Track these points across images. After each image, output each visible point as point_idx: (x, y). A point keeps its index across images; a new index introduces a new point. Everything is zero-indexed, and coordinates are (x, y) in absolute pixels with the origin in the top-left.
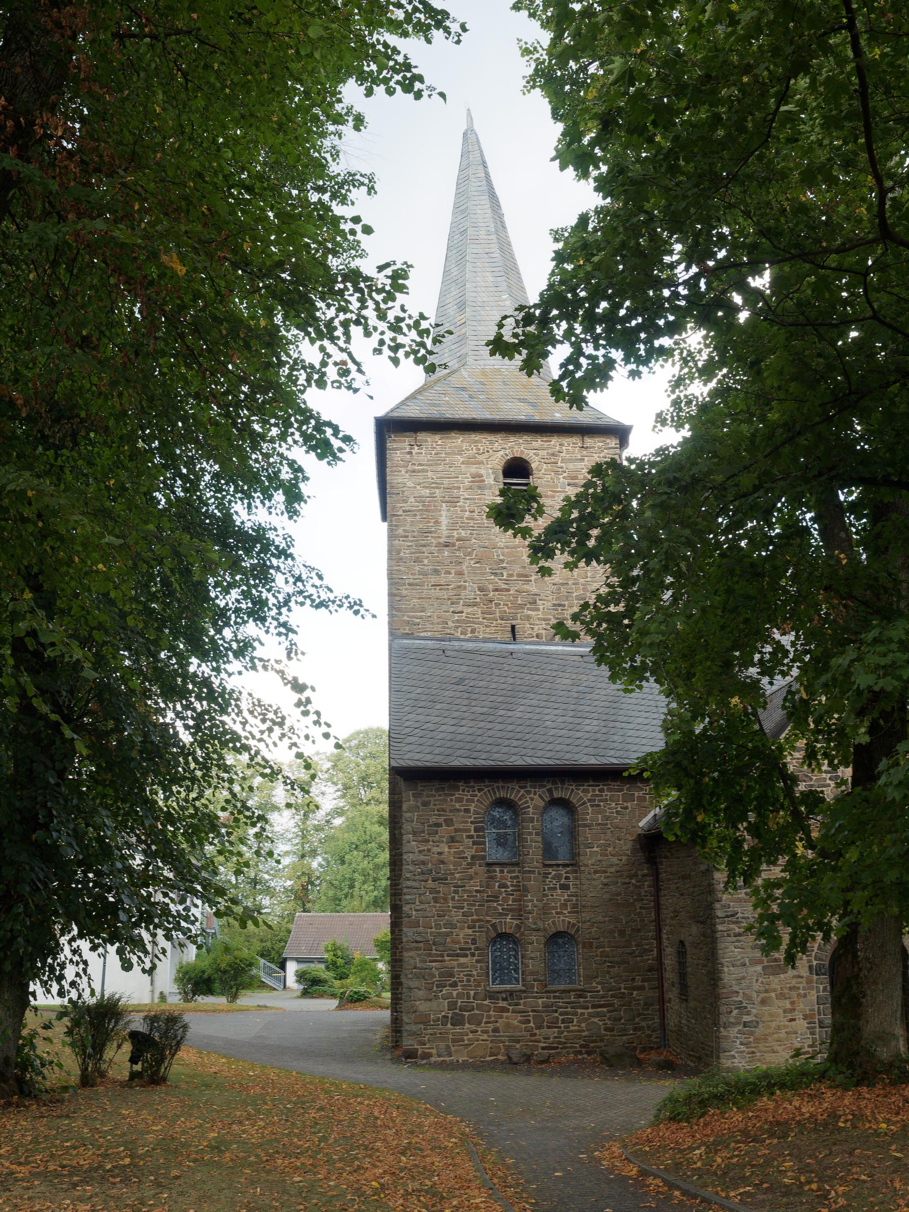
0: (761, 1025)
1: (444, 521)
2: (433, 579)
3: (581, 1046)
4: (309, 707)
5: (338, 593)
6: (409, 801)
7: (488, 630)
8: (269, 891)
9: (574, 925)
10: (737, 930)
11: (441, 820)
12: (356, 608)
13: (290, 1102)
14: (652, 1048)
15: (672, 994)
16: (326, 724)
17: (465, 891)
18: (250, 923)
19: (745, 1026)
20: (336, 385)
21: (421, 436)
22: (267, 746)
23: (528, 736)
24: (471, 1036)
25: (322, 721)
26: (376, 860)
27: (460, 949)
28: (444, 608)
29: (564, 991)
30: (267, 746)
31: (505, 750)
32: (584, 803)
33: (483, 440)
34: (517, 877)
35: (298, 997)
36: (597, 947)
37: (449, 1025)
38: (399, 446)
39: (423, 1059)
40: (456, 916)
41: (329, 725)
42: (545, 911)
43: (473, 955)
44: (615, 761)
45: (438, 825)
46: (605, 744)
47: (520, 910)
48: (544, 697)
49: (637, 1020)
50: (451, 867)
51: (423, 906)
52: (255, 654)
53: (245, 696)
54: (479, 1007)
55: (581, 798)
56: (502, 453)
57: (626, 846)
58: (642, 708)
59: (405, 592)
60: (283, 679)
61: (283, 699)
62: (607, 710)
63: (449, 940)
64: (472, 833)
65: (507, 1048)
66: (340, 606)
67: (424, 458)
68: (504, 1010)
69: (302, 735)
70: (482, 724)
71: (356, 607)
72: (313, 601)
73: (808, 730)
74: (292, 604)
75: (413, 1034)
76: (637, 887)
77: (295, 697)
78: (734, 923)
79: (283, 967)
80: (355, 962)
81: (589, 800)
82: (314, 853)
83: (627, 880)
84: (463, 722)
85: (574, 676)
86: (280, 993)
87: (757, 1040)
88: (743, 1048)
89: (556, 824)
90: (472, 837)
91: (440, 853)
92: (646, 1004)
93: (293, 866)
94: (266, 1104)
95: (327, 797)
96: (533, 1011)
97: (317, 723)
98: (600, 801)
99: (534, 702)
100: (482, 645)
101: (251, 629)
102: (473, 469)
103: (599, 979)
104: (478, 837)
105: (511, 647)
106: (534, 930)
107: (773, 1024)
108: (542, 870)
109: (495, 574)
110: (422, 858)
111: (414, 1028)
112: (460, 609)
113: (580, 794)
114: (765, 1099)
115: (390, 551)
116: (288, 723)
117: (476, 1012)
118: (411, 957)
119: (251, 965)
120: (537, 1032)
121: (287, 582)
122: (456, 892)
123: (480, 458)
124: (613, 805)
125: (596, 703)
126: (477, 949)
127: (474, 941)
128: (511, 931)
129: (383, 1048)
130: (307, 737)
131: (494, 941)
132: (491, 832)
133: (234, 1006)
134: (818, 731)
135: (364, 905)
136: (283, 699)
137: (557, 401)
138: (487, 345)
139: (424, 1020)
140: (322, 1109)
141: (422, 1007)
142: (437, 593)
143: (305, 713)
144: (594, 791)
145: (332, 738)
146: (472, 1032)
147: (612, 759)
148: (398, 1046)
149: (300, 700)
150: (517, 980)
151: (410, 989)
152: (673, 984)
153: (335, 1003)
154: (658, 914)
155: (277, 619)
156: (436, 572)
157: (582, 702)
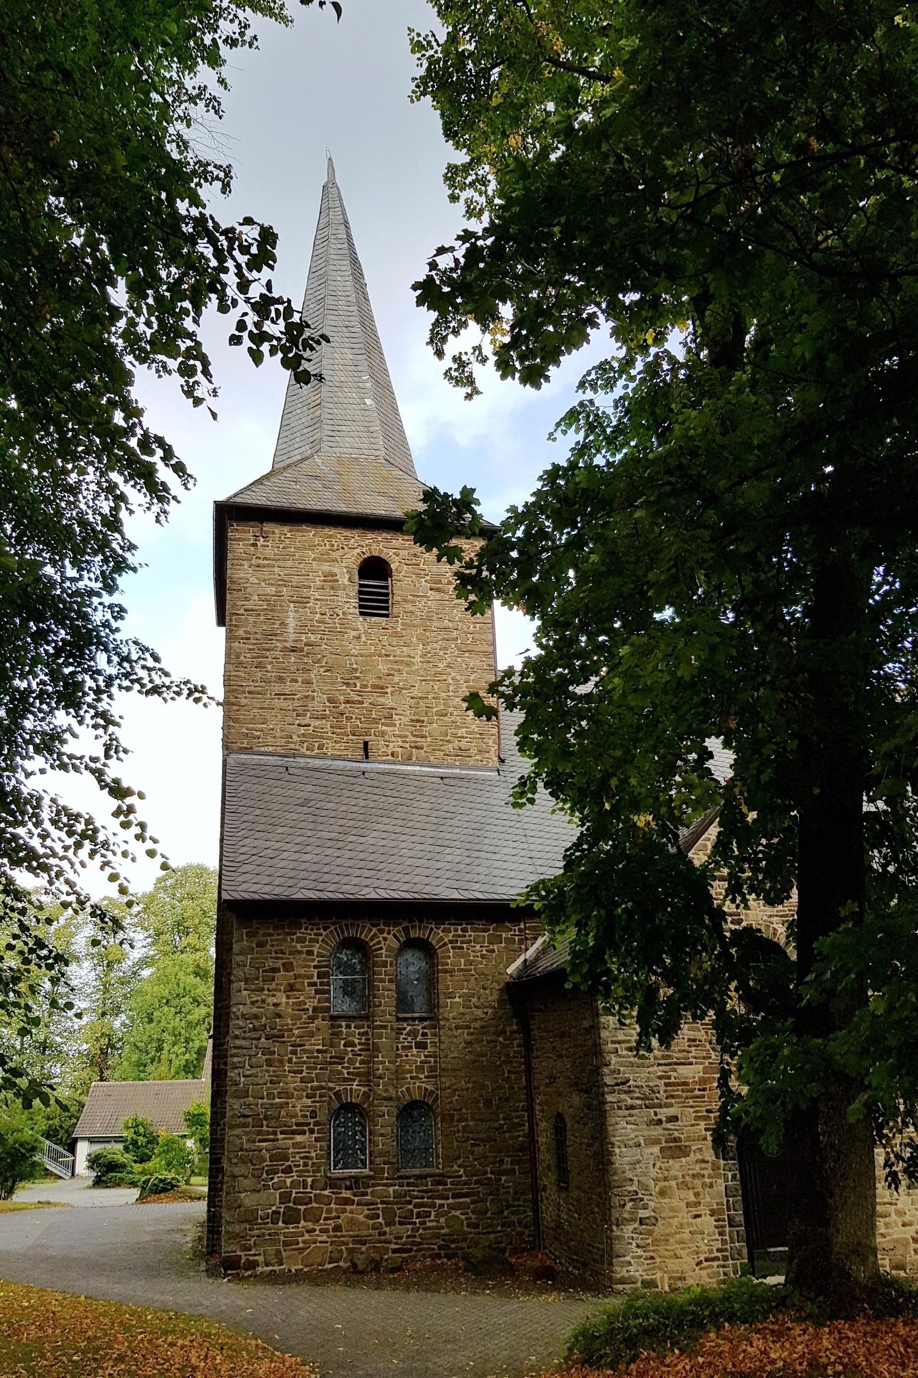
0: (660, 1222)
1: (292, 623)
2: (277, 688)
3: (440, 1248)
4: (131, 817)
5: (176, 677)
6: (241, 942)
7: (337, 746)
8: (60, 1056)
9: (432, 1092)
10: (629, 1102)
11: (279, 964)
12: (197, 695)
13: (77, 1350)
14: (524, 1250)
15: (548, 1180)
16: (151, 838)
17: (305, 1051)
18: (37, 1102)
19: (641, 1224)
20: (162, 518)
21: (268, 527)
22: (72, 864)
23: (381, 866)
24: (307, 1236)
25: (147, 835)
26: (189, 1017)
27: (297, 1124)
28: (289, 720)
29: (419, 1177)
30: (72, 864)
31: (356, 881)
32: (445, 945)
33: (338, 535)
34: (366, 1033)
35: (89, 1187)
36: (459, 1121)
37: (280, 1224)
38: (242, 538)
39: (247, 1270)
40: (293, 1082)
41: (155, 841)
42: (398, 1075)
43: (312, 1131)
44: (480, 896)
45: (275, 970)
46: (469, 877)
47: (369, 1074)
48: (400, 823)
49: (506, 1213)
50: (290, 1022)
51: (254, 1071)
52: (66, 749)
53: (46, 802)
54: (318, 1198)
55: (442, 939)
56: (358, 550)
57: (492, 996)
58: (509, 837)
59: (243, 701)
60: (100, 781)
61: (97, 805)
62: (470, 839)
63: (283, 1113)
64: (315, 979)
65: (351, 1251)
66: (178, 694)
67: (269, 552)
68: (347, 1202)
69: (119, 851)
70: (328, 852)
71: (196, 692)
72: (143, 686)
73: (732, 857)
74: (114, 690)
75: (234, 1236)
76: (506, 1046)
77: (114, 803)
78: (625, 1092)
79: (72, 1149)
80: (160, 1140)
81: (451, 942)
82: (117, 1011)
83: (493, 1038)
84: (308, 849)
85: (433, 800)
86: (67, 1183)
87: (656, 1242)
88: (640, 1252)
89: (411, 969)
90: (314, 984)
91: (276, 1005)
92: (516, 1192)
93: (91, 1026)
94: (43, 1357)
95: (139, 944)
96: (382, 1202)
97: (140, 837)
98: (463, 942)
99: (387, 828)
100: (330, 762)
101: (62, 718)
102: (326, 567)
103: (459, 1162)
104: (322, 984)
105: (363, 766)
106: (385, 1099)
107: (675, 1222)
108: (395, 1025)
109: (348, 684)
110: (255, 1010)
111: (237, 1228)
112: (306, 722)
113: (442, 935)
114: (712, 1335)
115: (228, 654)
116: (101, 837)
117: (315, 1205)
118: (236, 1137)
119: (34, 1149)
120: (387, 1229)
121: (109, 661)
122: (294, 1053)
123: (335, 555)
124: (478, 947)
125: (457, 830)
126: (316, 1124)
127: (313, 1114)
128: (358, 1101)
129: (197, 1255)
130: (125, 854)
131: (336, 1114)
132: (337, 978)
133: (8, 1203)
134: (742, 859)
135: (173, 1071)
136: (97, 805)
137: (503, 377)
138: (415, 287)
139: (250, 1218)
140: (121, 1359)
141: (248, 1200)
142: (279, 703)
143: (125, 825)
144: (456, 930)
145: (158, 857)
146: (308, 1232)
147: (477, 892)
148: (218, 1252)
149: (119, 807)
150: (363, 1163)
151: (234, 1177)
152: (549, 1168)
153: (136, 1192)
154: (529, 1081)
155: (94, 708)
156: (281, 679)
157: (442, 828)
